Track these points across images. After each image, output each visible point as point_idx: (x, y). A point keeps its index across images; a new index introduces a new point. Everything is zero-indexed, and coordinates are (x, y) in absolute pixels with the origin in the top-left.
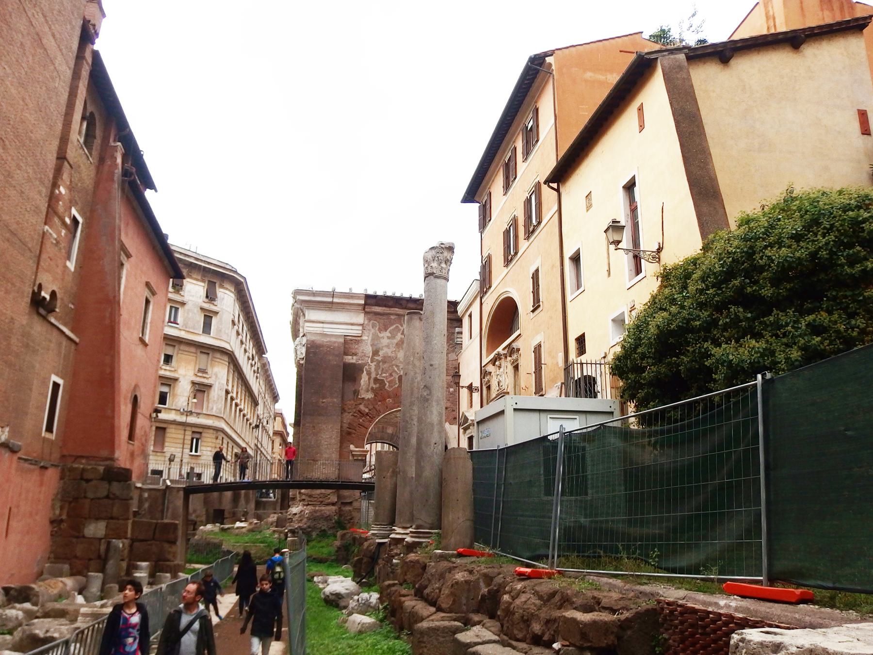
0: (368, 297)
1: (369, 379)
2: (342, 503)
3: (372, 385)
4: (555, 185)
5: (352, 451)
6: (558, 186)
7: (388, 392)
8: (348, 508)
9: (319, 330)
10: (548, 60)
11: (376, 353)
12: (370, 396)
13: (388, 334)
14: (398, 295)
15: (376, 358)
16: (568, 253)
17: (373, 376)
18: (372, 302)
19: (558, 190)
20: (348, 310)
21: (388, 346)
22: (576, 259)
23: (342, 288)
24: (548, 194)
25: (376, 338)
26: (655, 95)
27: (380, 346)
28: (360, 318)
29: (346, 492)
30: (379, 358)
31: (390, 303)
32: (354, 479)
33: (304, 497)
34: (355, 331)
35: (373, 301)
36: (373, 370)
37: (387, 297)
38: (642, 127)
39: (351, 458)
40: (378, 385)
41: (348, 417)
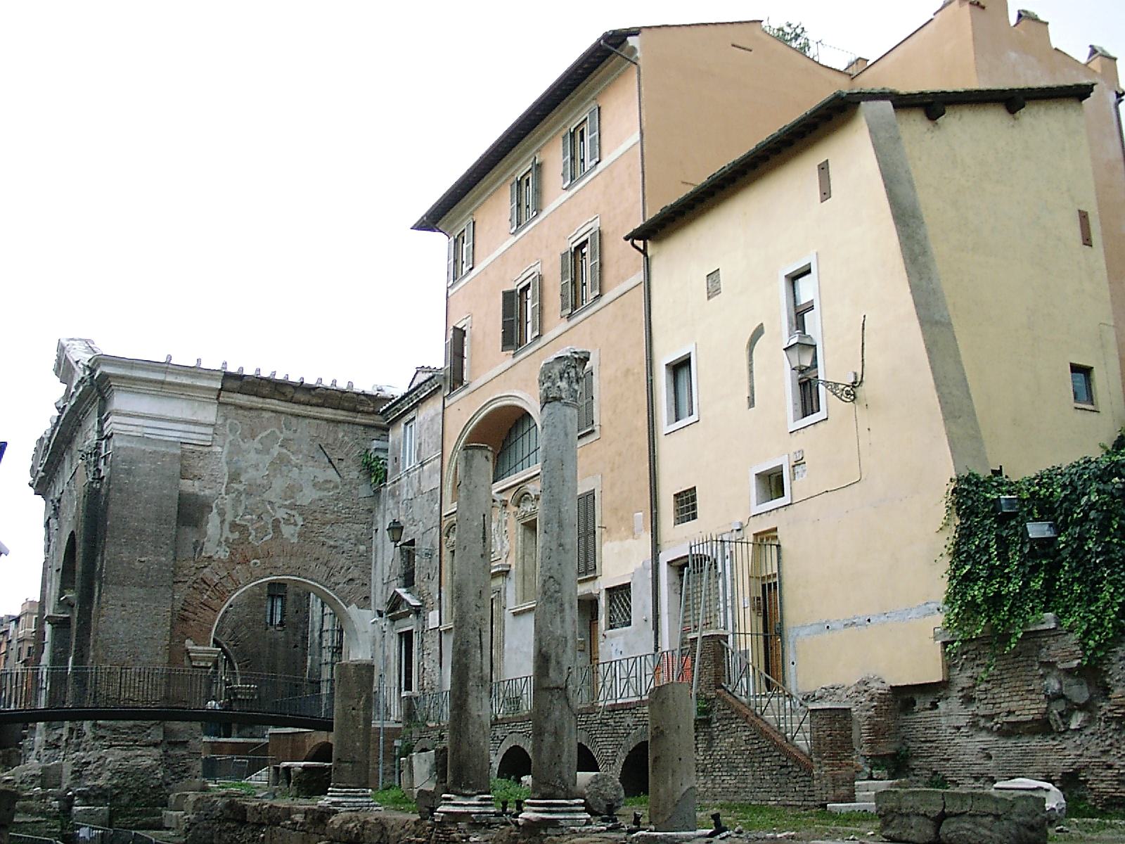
0: (228, 376)
1: (222, 522)
2: (169, 743)
3: (227, 533)
4: (640, 244)
5: (188, 652)
6: (645, 245)
7: (254, 548)
8: (179, 752)
9: (136, 432)
10: (632, 41)
11: (234, 477)
12: (223, 554)
13: (256, 444)
14: (279, 376)
15: (235, 486)
16: (666, 355)
17: (229, 517)
18: (235, 383)
19: (644, 252)
20: (190, 398)
21: (256, 467)
22: (680, 367)
23: (184, 358)
24: (621, 255)
25: (235, 450)
26: (853, 153)
27: (243, 464)
28: (209, 413)
29: (177, 726)
30: (241, 487)
31: (266, 391)
32: (194, 706)
33: (101, 733)
34: (198, 435)
35: (236, 384)
36: (228, 508)
37: (262, 379)
38: (826, 194)
39: (186, 662)
40: (236, 535)
41: (182, 593)
